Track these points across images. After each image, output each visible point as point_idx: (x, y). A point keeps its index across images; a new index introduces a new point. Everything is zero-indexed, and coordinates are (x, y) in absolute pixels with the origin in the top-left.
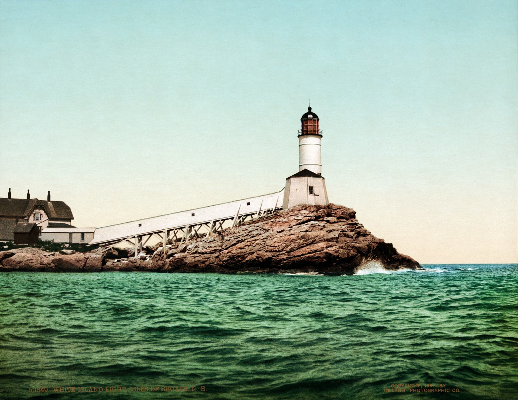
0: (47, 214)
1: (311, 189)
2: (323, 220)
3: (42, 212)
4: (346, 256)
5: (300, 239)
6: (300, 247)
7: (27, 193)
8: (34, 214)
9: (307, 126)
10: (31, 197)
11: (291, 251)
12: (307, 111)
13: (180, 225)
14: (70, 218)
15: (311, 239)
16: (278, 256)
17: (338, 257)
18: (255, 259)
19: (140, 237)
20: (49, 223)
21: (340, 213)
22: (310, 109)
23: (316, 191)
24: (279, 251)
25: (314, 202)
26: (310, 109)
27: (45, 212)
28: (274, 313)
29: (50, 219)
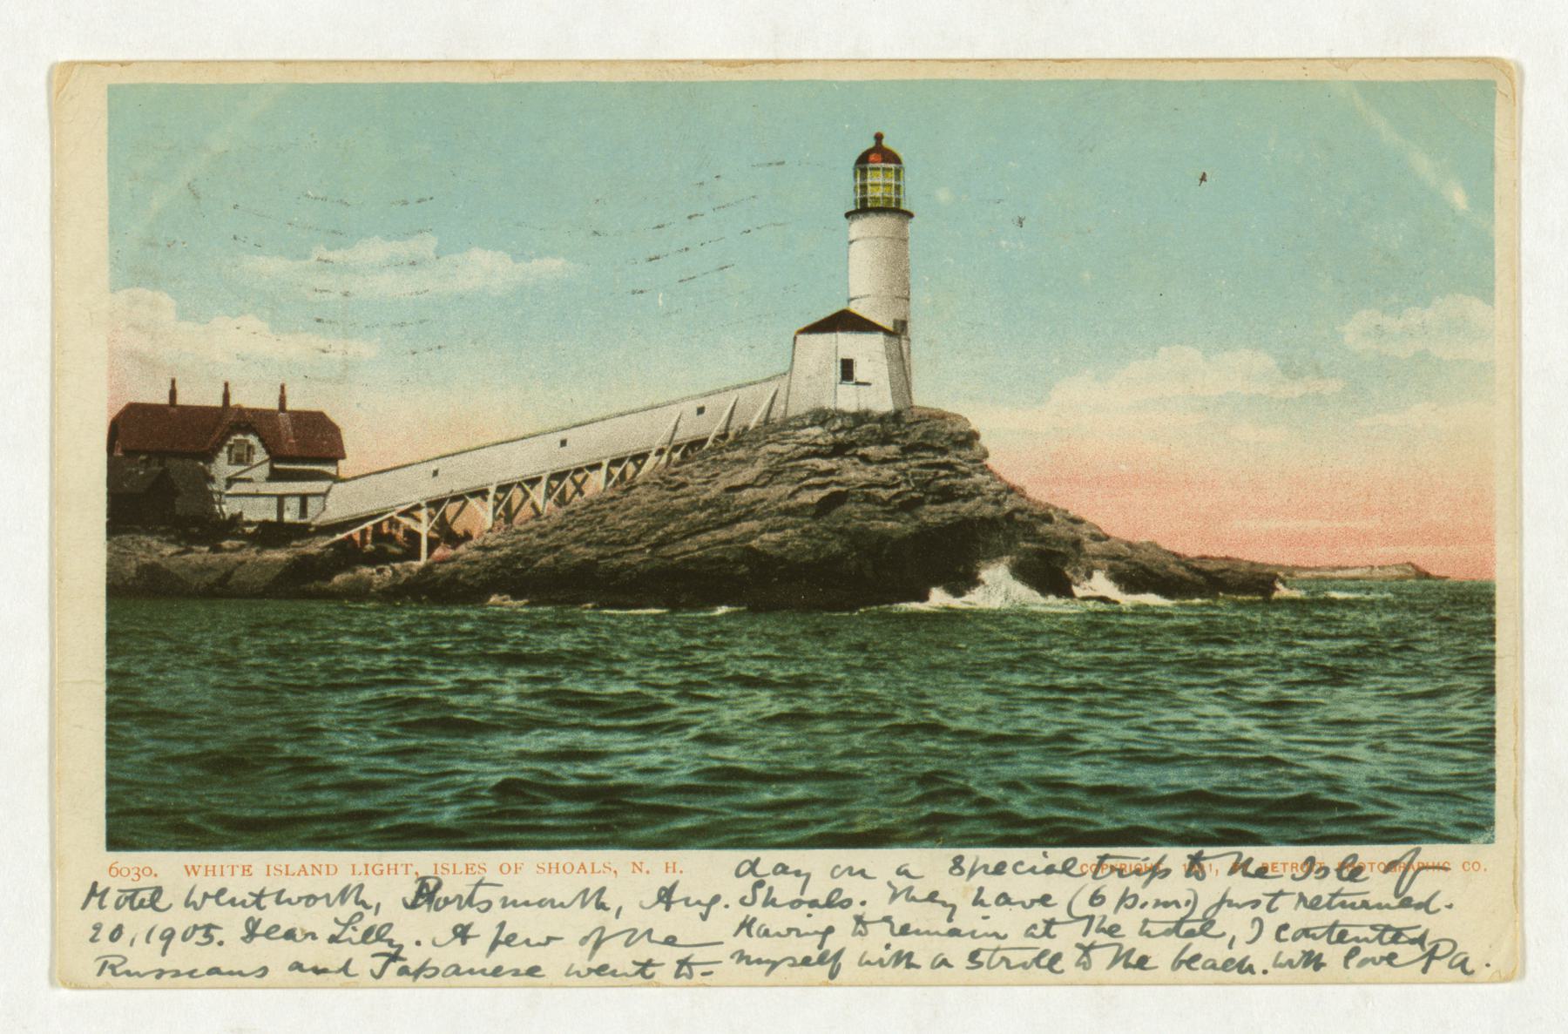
0: (265, 446)
1: (847, 369)
2: (855, 455)
3: (253, 440)
4: (809, 558)
5: (702, 509)
6: (694, 531)
7: (278, 393)
8: (231, 447)
9: (864, 187)
10: (233, 402)
11: (661, 543)
12: (871, 144)
13: (530, 471)
14: (334, 453)
15: (736, 508)
16: (616, 556)
17: (782, 559)
18: (837, 559)
19: (436, 504)
20: (272, 470)
21: (916, 436)
22: (879, 137)
23: (859, 373)
24: (623, 543)
25: (854, 400)
26: (879, 137)
27: (261, 440)
28: (1270, 718)
29: (275, 457)
